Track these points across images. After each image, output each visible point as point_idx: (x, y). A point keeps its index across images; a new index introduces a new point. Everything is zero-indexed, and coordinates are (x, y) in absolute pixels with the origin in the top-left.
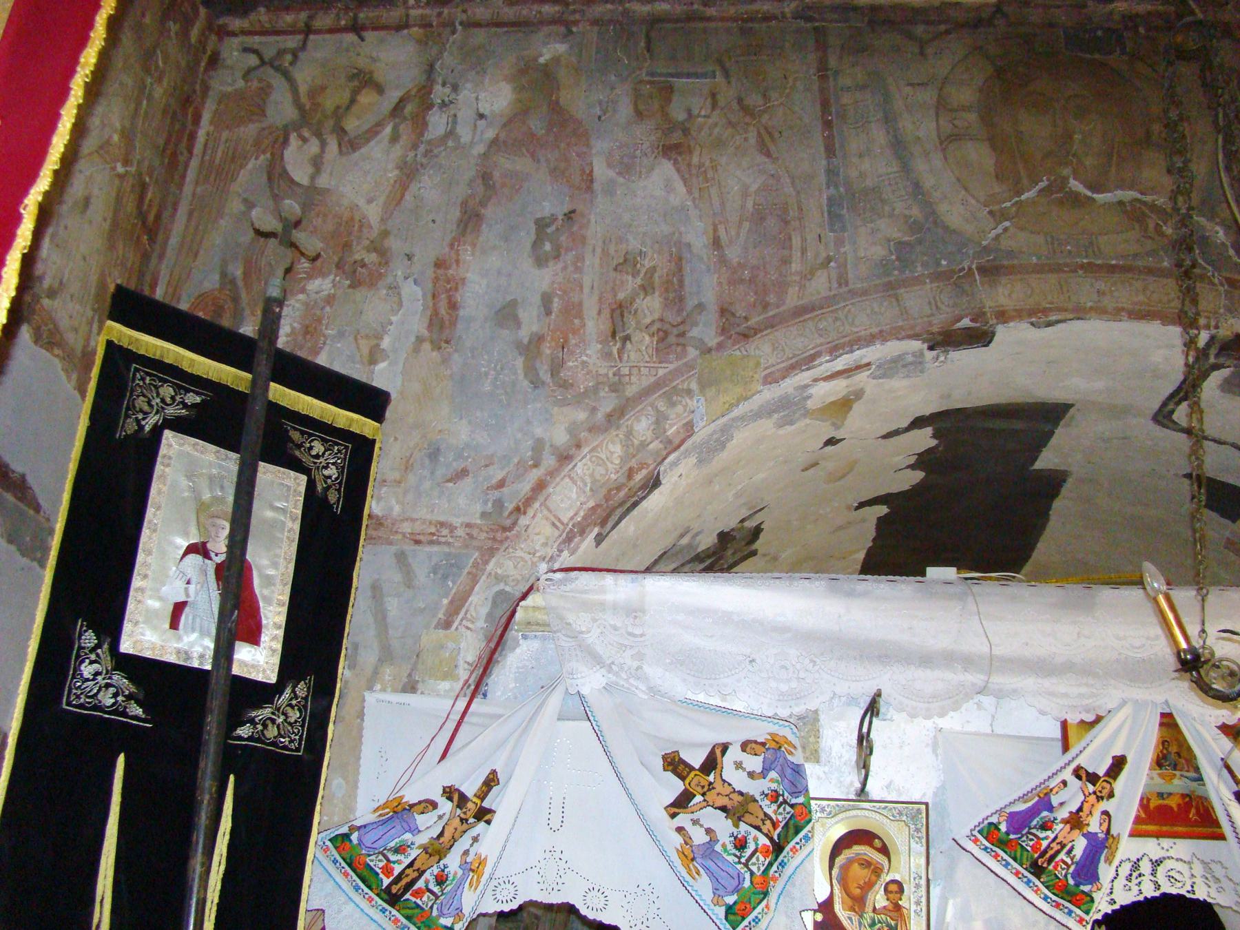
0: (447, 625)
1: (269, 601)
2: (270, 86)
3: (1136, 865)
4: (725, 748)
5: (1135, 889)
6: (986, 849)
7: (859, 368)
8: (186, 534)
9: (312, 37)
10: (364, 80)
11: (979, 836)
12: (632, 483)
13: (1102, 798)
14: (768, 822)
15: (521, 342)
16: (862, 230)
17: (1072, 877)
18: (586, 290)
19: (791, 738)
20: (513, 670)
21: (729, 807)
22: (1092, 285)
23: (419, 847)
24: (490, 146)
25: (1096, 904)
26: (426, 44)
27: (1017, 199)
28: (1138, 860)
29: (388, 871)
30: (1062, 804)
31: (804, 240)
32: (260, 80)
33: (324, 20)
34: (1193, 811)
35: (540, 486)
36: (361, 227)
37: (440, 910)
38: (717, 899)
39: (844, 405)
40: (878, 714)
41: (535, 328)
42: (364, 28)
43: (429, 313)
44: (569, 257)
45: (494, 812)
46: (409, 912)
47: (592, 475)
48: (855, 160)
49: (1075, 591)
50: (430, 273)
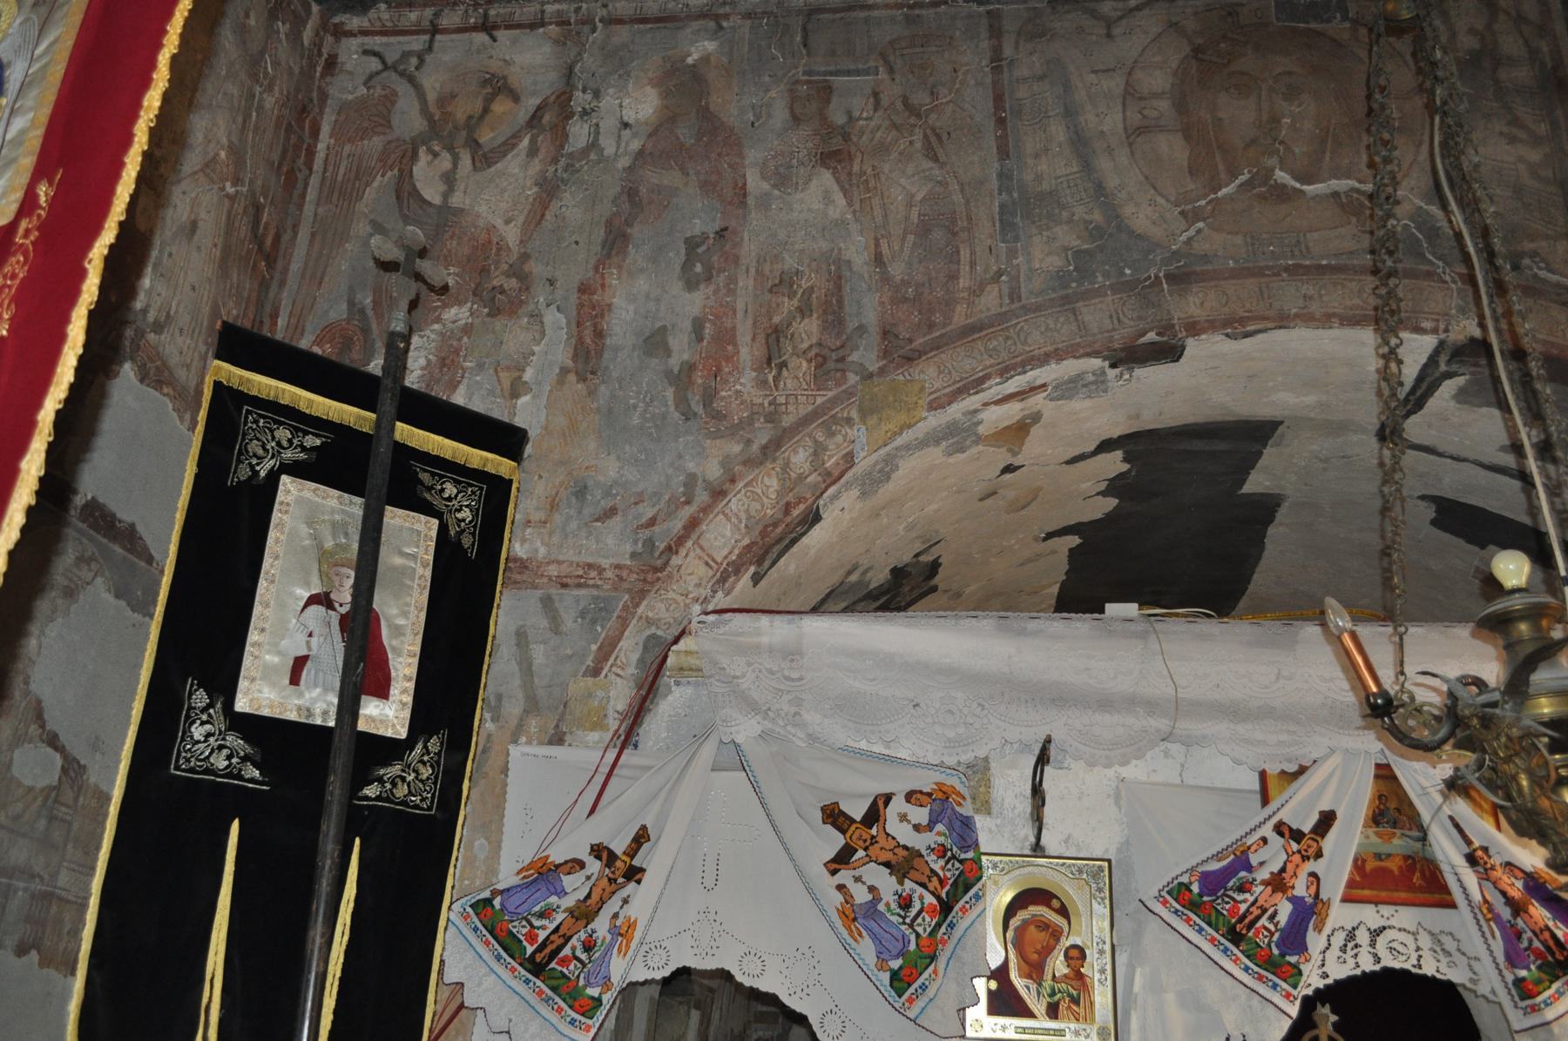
0: (596, 672)
1: (398, 652)
2: (395, 94)
3: (1351, 935)
4: (888, 798)
5: (1351, 962)
6: (1176, 912)
7: (1033, 389)
8: (307, 584)
9: (438, 37)
10: (498, 86)
11: (1168, 898)
12: (789, 519)
13: (1308, 858)
14: (935, 879)
15: (672, 371)
16: (1037, 239)
17: (1277, 946)
18: (740, 315)
19: (959, 787)
20: (666, 719)
21: (893, 862)
22: (1297, 290)
23: (565, 911)
24: (636, 159)
25: (1304, 978)
26: (565, 44)
27: (1213, 196)
28: (1354, 929)
29: (531, 937)
30: (1262, 864)
31: (973, 253)
32: (384, 87)
33: (450, 19)
34: (1418, 874)
35: (693, 524)
36: (499, 250)
37: (587, 979)
38: (881, 964)
39: (1020, 430)
40: (1048, 762)
41: (686, 357)
42: (495, 27)
43: (573, 341)
44: (721, 279)
45: (644, 870)
46: (555, 983)
47: (747, 511)
48: (1030, 161)
49: (1272, 627)
50: (574, 298)
